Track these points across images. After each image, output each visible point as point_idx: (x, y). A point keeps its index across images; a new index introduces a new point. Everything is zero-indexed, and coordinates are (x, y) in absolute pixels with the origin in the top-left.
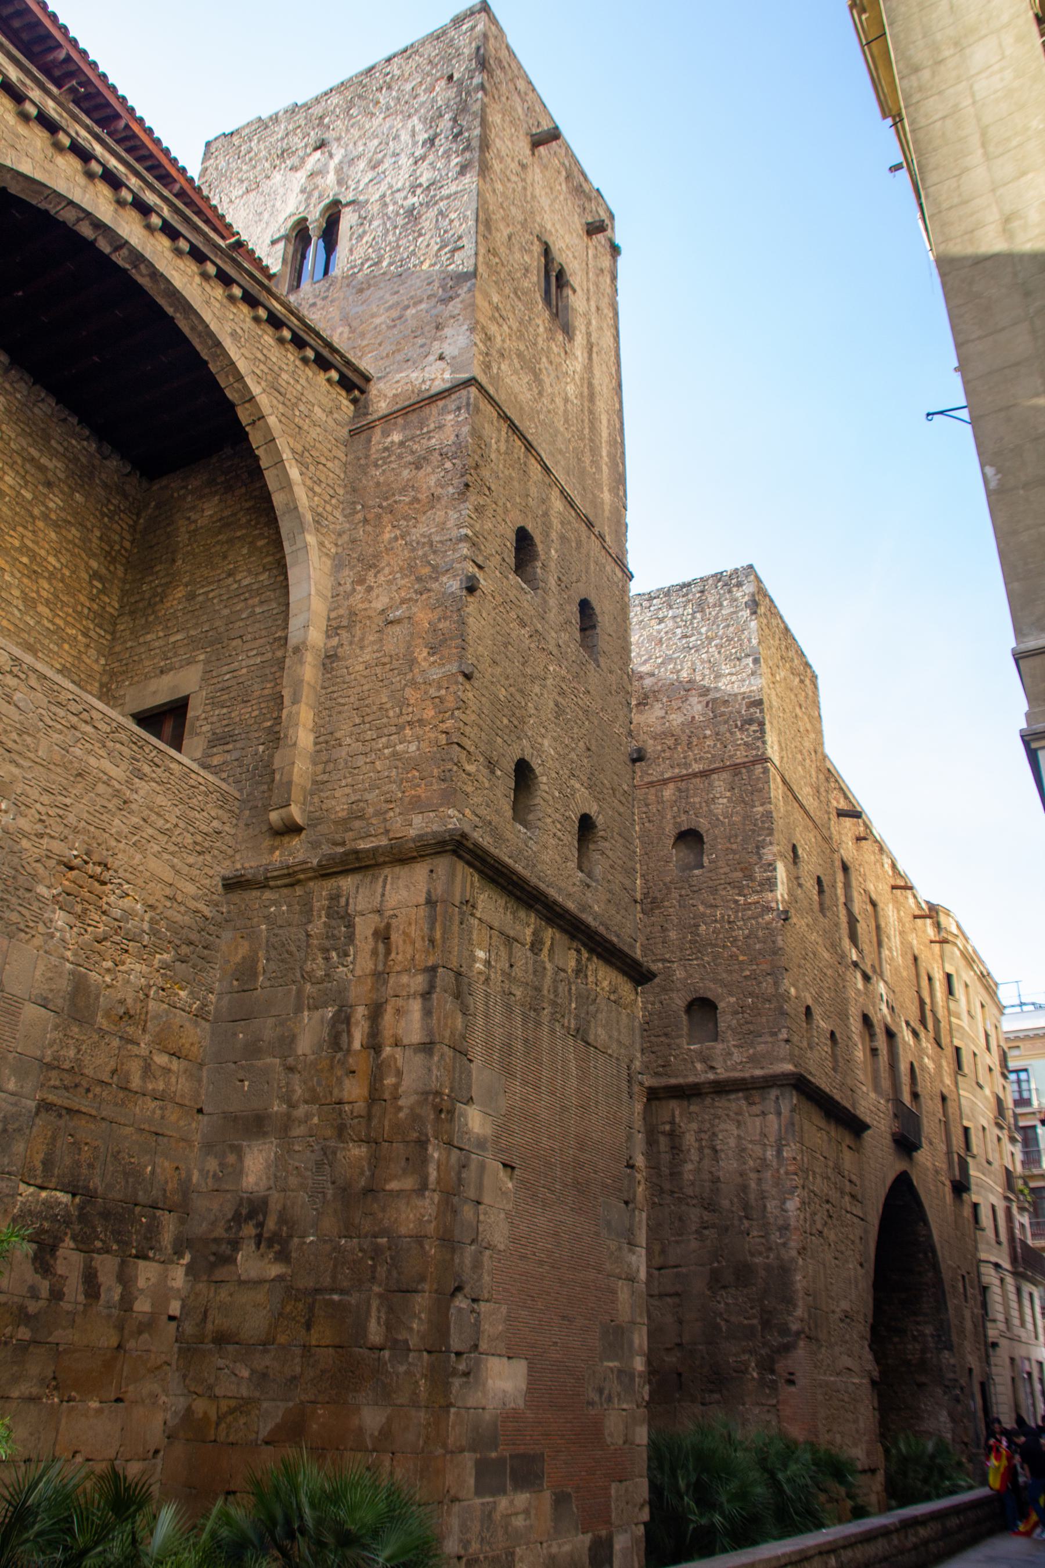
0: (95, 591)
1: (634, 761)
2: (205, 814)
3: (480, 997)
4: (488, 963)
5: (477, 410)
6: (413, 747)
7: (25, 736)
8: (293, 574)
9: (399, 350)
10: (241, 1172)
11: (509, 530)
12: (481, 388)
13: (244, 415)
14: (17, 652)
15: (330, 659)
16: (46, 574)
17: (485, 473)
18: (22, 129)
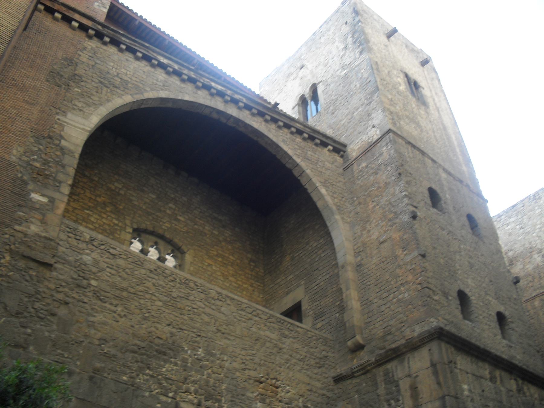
0: (252, 267)
5: (395, 142)
6: (406, 295)
8: (334, 234)
9: (355, 130)
12: (394, 133)
13: (296, 173)
14: (219, 290)
16: (230, 264)
17: (406, 167)
18: (183, 85)
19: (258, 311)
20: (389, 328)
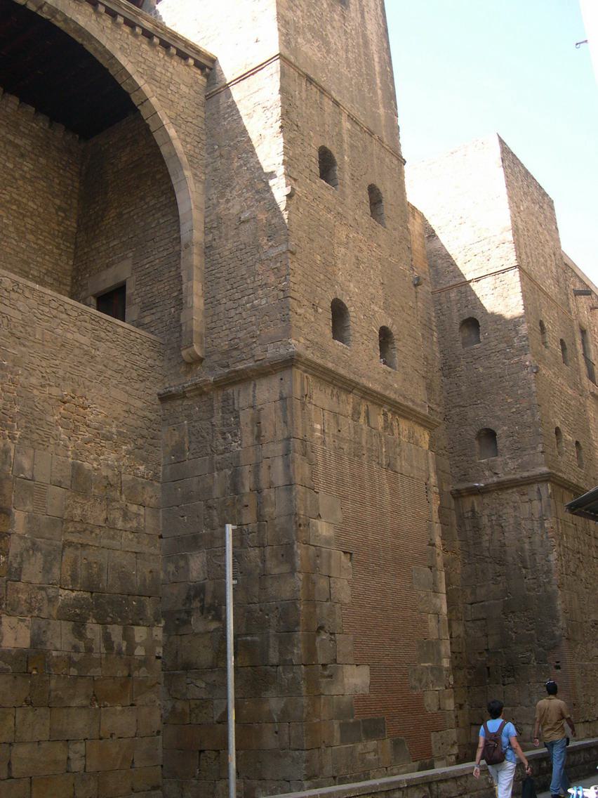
0: (60, 219)
1: (416, 286)
2: (143, 356)
3: (319, 454)
4: (323, 431)
6: (264, 302)
7: (27, 328)
8: (180, 197)
10: (188, 570)
11: (313, 151)
15: (208, 249)
19: (66, 306)
20: (236, 340)
